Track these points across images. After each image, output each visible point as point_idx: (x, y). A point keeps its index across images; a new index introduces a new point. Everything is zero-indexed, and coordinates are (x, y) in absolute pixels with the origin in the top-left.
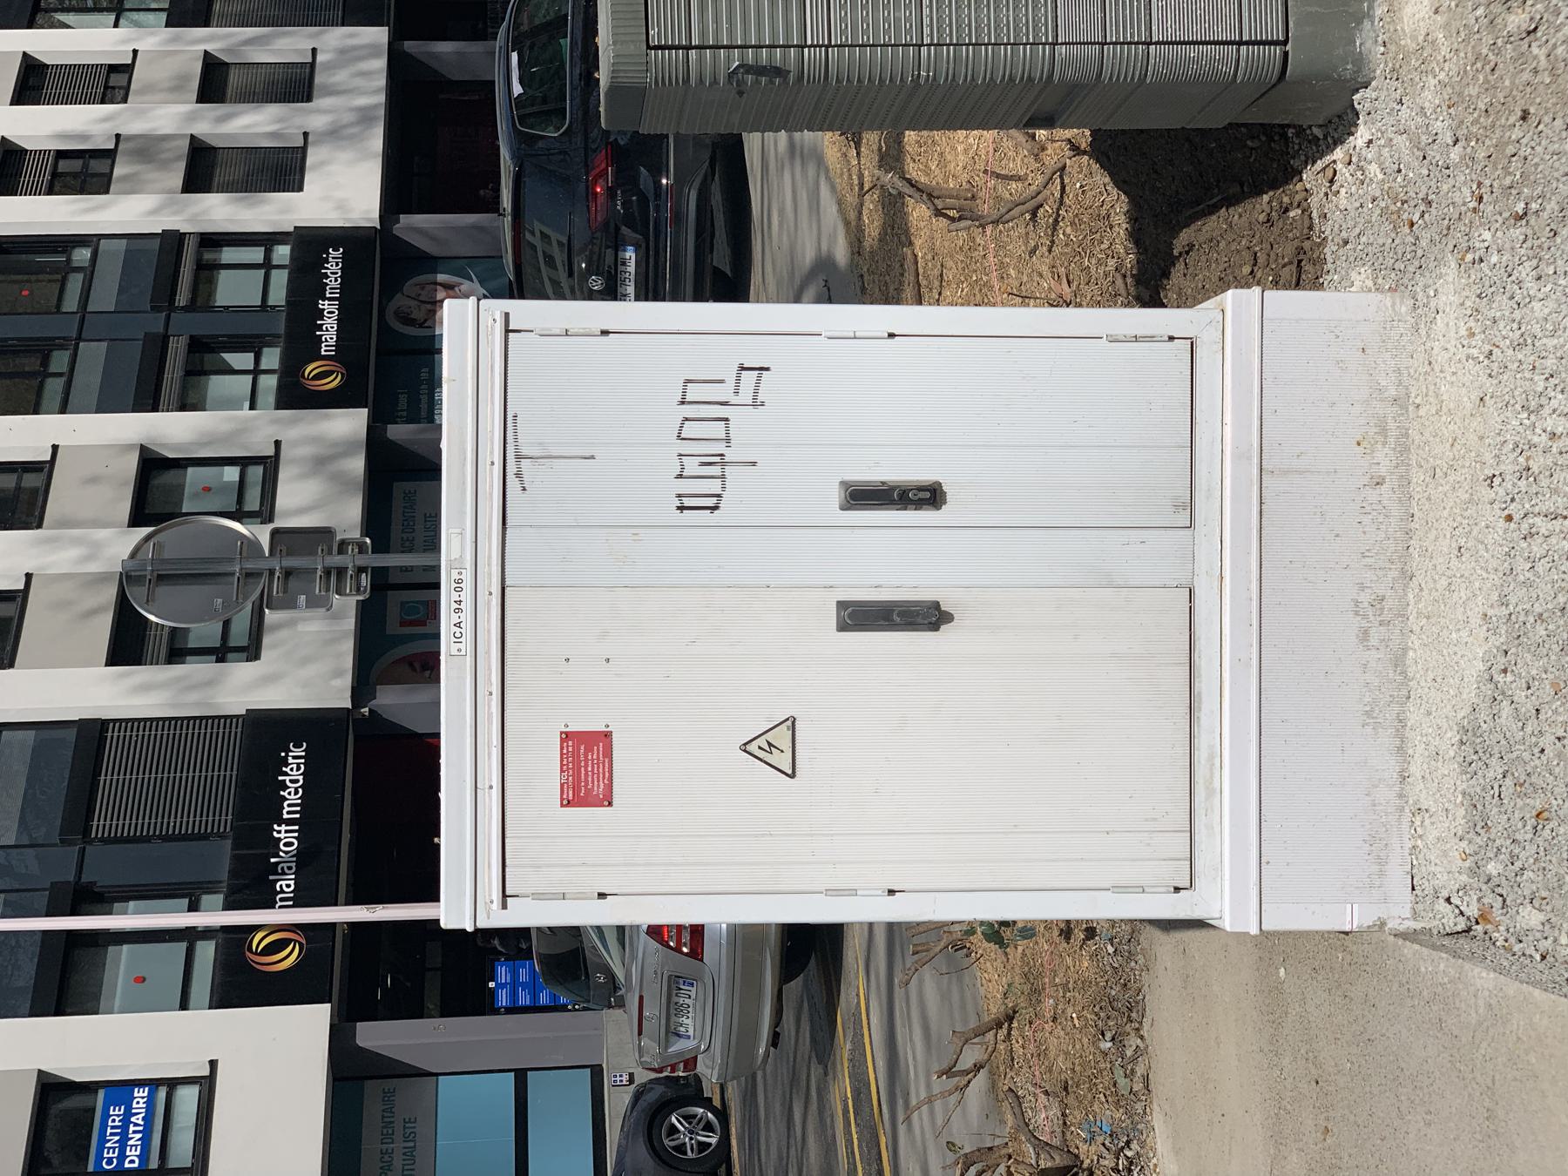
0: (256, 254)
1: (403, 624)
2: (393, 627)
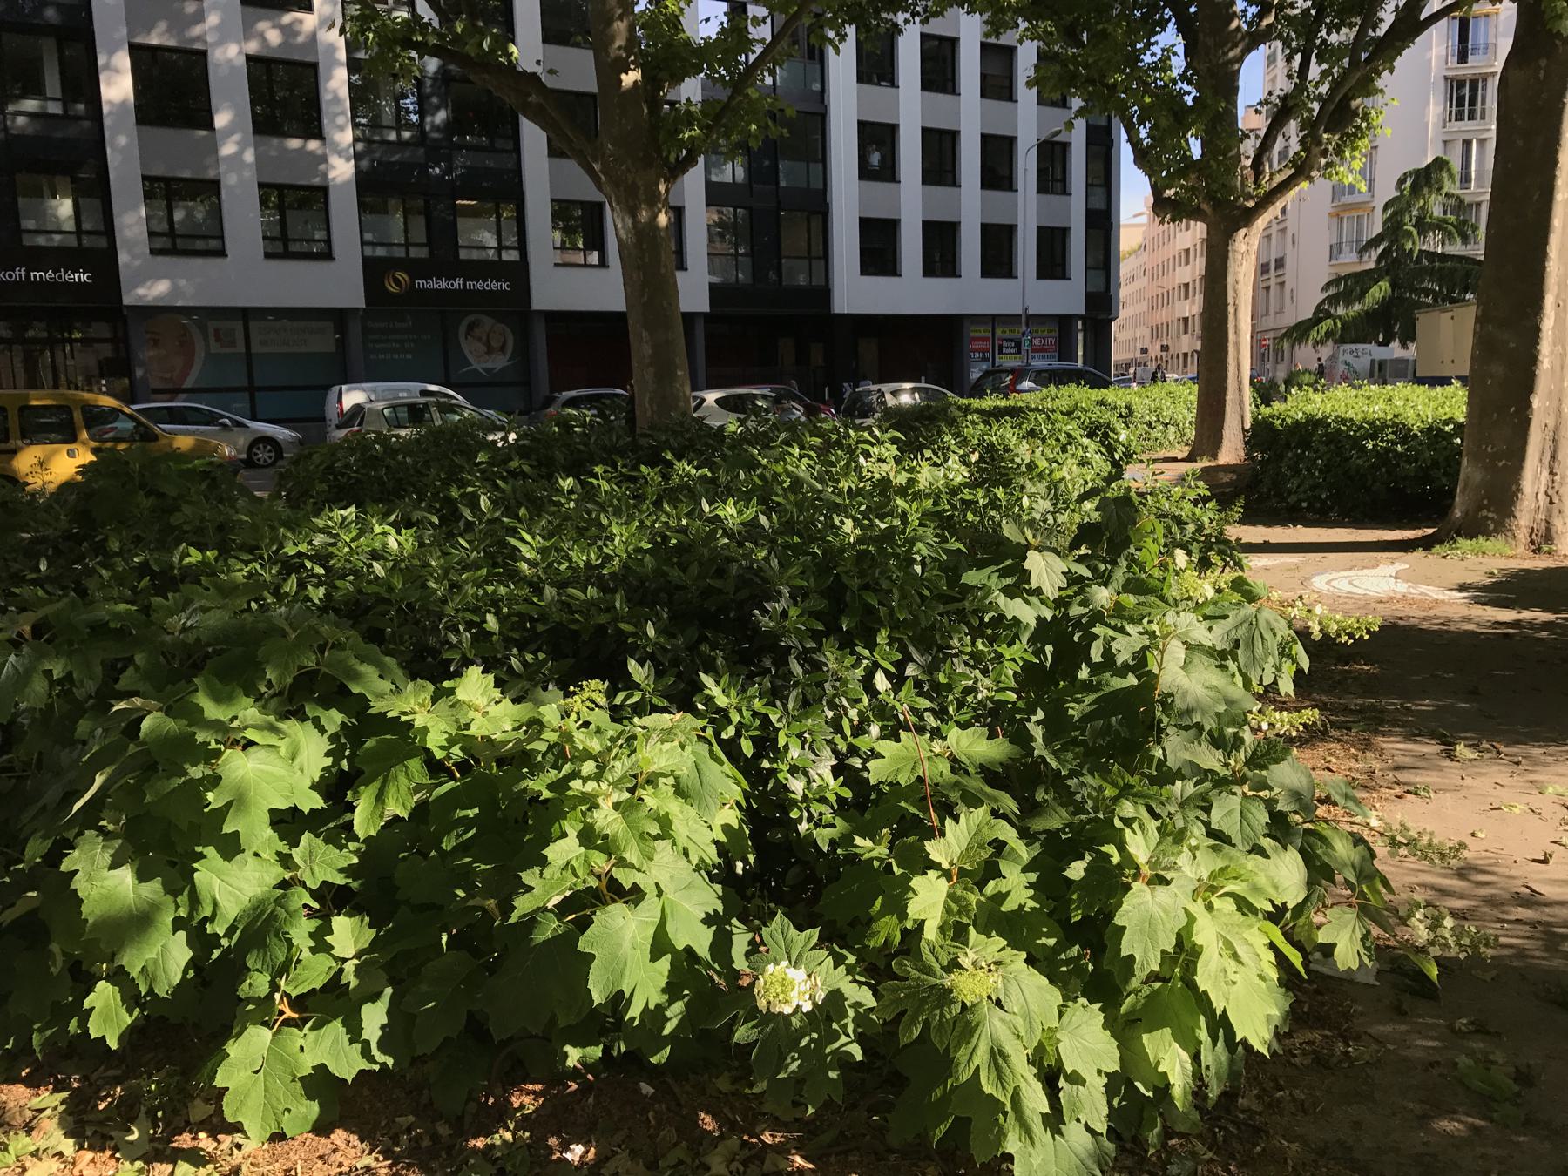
0: (295, 247)
1: (217, 331)
2: (212, 325)
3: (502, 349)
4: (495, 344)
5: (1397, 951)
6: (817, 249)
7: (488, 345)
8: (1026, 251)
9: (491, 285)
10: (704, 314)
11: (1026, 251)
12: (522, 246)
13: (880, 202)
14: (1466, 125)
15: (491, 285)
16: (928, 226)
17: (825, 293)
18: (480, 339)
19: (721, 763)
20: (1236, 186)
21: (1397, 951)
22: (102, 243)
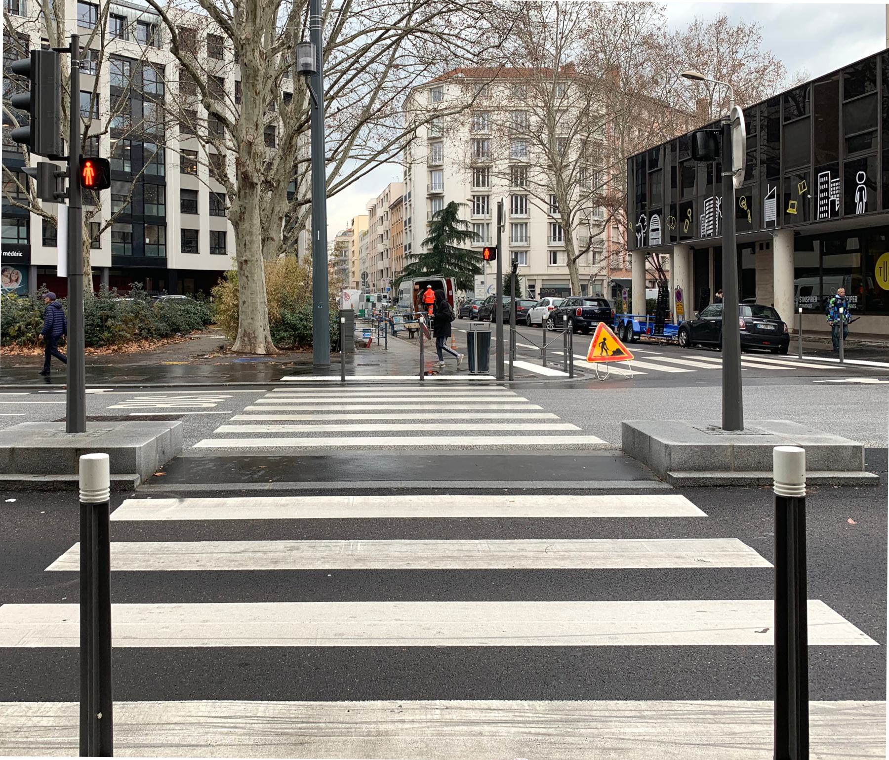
3: (17, 280)
4: (13, 278)
5: (224, 16)
6: (162, 241)
7: (10, 279)
8: (204, 242)
9: (14, 254)
10: (109, 268)
11: (204, 242)
12: (28, 238)
13: (190, 222)
14: (481, 216)
15: (14, 254)
16: (212, 233)
17: (164, 260)
18: (7, 276)
19: (295, 363)
20: (452, 313)
21: (224, 16)
22: (26, 242)
